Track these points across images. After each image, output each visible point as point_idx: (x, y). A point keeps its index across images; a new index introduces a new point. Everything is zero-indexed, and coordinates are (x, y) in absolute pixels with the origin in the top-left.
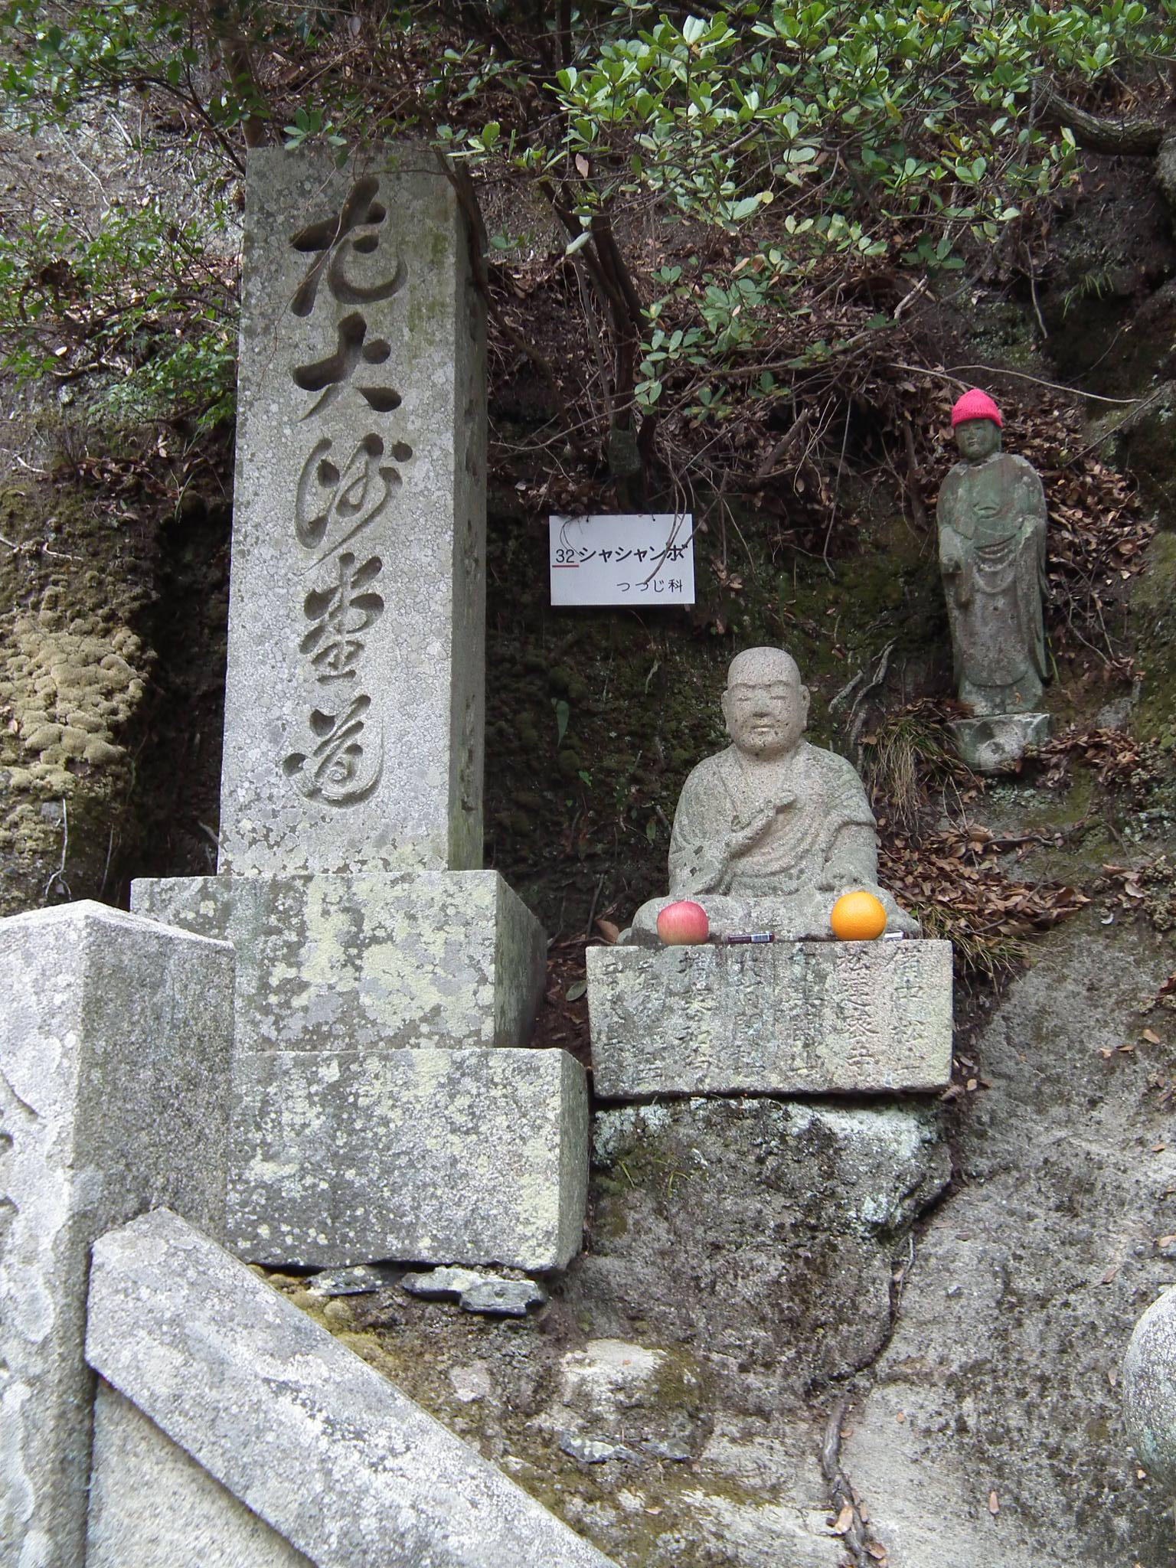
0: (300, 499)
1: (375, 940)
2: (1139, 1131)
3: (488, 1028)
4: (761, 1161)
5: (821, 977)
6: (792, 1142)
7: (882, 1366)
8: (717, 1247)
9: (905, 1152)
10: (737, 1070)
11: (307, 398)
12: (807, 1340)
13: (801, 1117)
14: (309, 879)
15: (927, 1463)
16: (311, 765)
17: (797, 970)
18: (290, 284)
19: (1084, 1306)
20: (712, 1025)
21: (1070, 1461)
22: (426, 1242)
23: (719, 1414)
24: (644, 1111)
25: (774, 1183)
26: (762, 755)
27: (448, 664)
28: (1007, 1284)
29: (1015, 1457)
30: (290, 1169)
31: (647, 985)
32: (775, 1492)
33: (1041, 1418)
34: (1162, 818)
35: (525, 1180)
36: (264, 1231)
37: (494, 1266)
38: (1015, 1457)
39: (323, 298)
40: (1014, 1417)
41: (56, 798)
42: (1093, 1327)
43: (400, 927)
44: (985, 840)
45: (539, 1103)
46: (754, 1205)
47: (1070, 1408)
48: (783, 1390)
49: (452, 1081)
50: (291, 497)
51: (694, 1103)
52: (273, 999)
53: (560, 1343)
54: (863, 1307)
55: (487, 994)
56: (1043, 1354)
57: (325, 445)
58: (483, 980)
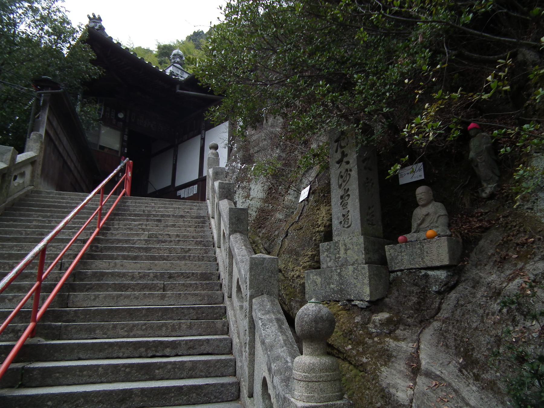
3: (364, 261)
4: (414, 281)
5: (423, 247)
7: (435, 318)
8: (406, 296)
10: (411, 264)
11: (338, 165)
13: (423, 272)
16: (343, 223)
18: (335, 149)
20: (406, 257)
25: (416, 285)
26: (424, 206)
29: (448, 335)
32: (404, 340)
37: (362, 300)
38: (448, 335)
39: (339, 149)
40: (450, 328)
41: (322, 232)
42: (469, 311)
43: (351, 246)
45: (95, 295)
51: (405, 271)
53: (373, 313)
55: (364, 256)
57: (341, 172)
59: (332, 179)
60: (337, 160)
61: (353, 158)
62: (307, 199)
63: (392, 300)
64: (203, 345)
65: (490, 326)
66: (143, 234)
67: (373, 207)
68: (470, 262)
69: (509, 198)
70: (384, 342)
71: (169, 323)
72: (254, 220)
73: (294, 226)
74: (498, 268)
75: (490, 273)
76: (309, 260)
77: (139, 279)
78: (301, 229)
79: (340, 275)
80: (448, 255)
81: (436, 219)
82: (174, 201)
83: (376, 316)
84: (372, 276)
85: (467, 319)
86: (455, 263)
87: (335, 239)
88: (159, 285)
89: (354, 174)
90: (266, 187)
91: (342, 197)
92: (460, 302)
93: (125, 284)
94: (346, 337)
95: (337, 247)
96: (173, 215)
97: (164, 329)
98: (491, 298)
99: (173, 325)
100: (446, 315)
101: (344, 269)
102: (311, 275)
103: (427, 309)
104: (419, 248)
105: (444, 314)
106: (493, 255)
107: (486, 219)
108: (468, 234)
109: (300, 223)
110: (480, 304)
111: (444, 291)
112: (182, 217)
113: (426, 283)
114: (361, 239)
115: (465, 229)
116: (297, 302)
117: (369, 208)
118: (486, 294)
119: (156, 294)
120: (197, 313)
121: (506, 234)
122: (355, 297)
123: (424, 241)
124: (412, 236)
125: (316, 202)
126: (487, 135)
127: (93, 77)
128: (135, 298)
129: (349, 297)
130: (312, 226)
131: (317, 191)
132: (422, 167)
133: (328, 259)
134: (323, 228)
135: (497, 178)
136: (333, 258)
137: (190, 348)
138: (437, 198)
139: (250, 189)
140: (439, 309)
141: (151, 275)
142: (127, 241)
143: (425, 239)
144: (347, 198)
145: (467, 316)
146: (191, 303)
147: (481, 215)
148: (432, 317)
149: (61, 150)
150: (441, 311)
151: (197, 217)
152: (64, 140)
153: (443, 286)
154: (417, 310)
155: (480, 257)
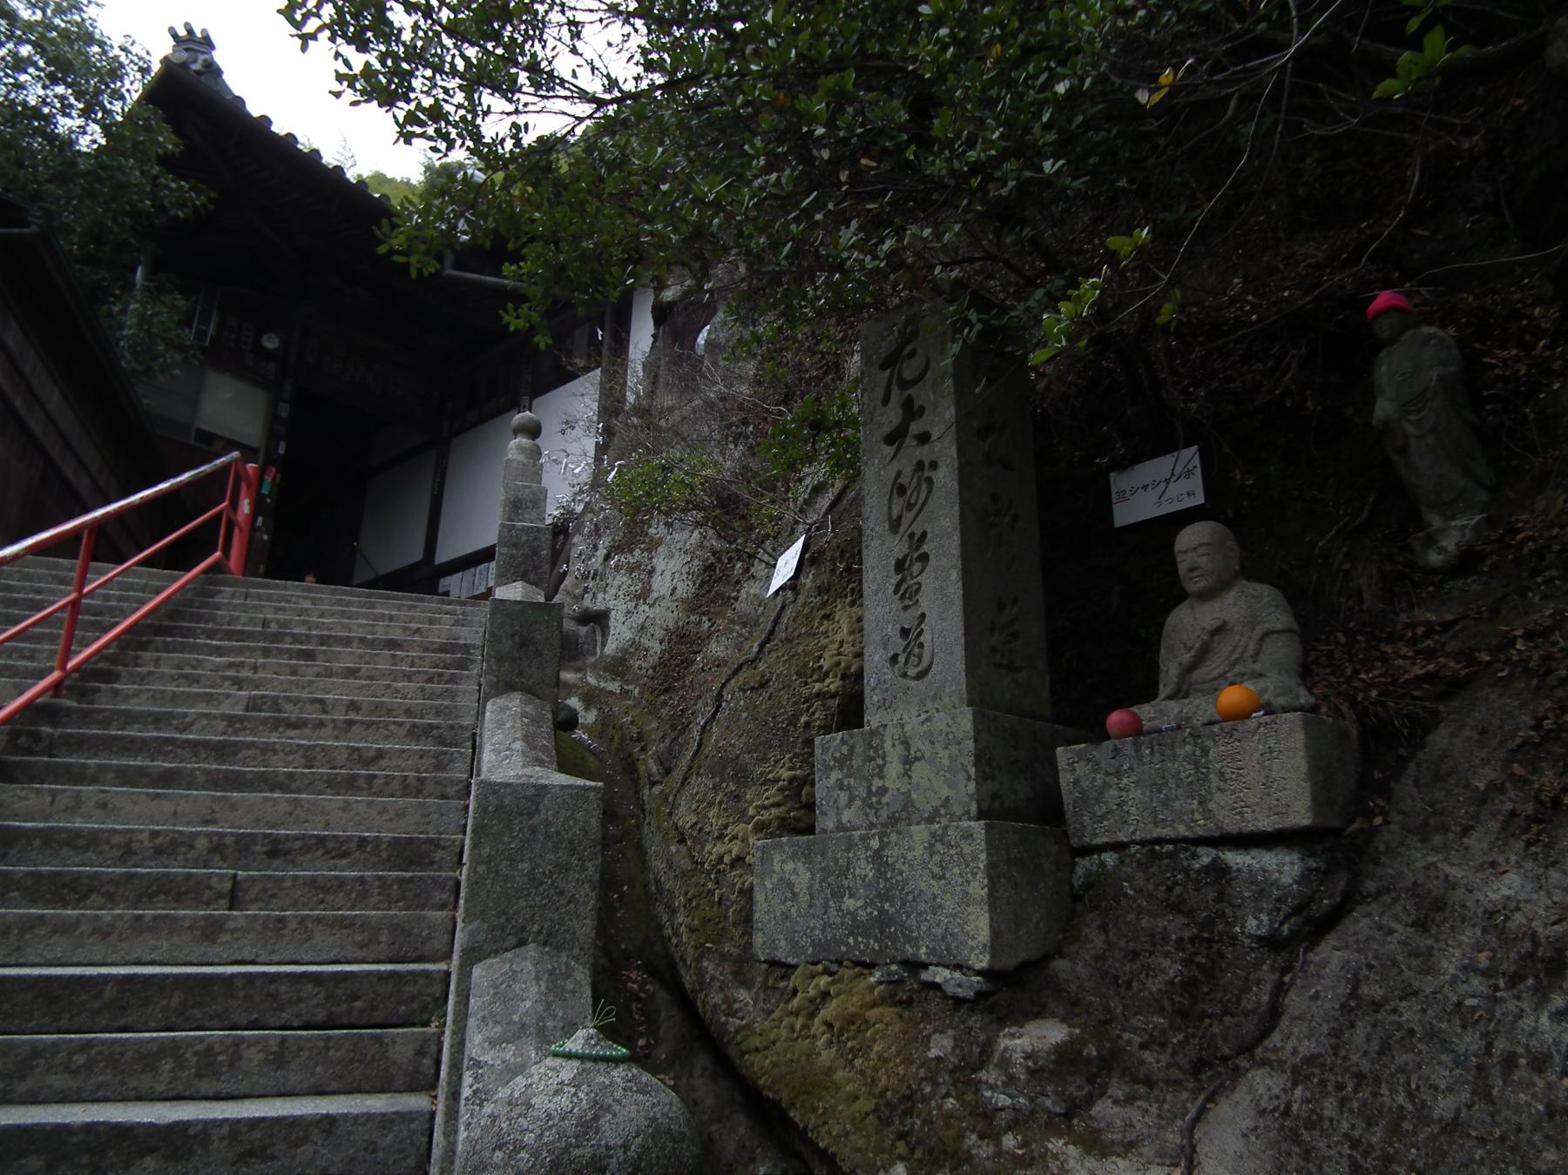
0: (890, 508)
1: (917, 759)
2: (1494, 855)
3: (974, 808)
4: (1170, 890)
5: (1205, 751)
6: (1193, 875)
7: (1259, 1051)
8: (1135, 955)
9: (1286, 880)
11: (889, 450)
12: (1196, 1027)
13: (1206, 856)
14: (885, 726)
15: (1253, 1139)
16: (902, 659)
17: (1188, 748)
18: (880, 391)
19: (1409, 1013)
20: (1136, 794)
21: (1366, 1154)
22: (923, 950)
23: (1115, 1081)
24: (1103, 856)
25: (1176, 907)
26: (1206, 596)
27: (960, 584)
28: (1354, 989)
30: (860, 903)
31: (1094, 771)
33: (1351, 1111)
34: (1554, 578)
35: (971, 909)
36: (851, 940)
37: (958, 967)
39: (895, 391)
40: (1329, 1108)
41: (833, 696)
42: (1412, 1032)
43: (926, 748)
44: (1427, 623)
45: (975, 858)
46: (1162, 923)
47: (1377, 1105)
48: (1168, 1066)
49: (931, 845)
50: (885, 509)
51: (1134, 848)
52: (874, 799)
53: (1002, 1021)
54: (1244, 1003)
55: (972, 786)
56: (1365, 1053)
57: (899, 474)
58: (969, 779)
59: (868, 500)
60: (887, 429)
61: (942, 417)
62: (793, 584)
63: (1081, 970)
64: (305, 1140)
65: (1525, 1120)
66: (228, 696)
67: (1014, 601)
68: (1396, 817)
69: (1549, 558)
70: (1043, 1156)
71: (190, 1043)
72: (654, 668)
73: (742, 676)
74: (1529, 844)
75: (1493, 865)
76: (778, 798)
77: (152, 858)
78: (764, 685)
79: (878, 858)
80: (1307, 785)
81: (1252, 647)
82: (380, 596)
83: (1012, 1036)
84: (1003, 867)
85: (1402, 1070)
86: (1335, 823)
87: (872, 719)
88: (214, 881)
89: (946, 477)
90: (696, 562)
91: (900, 566)
92: (1364, 990)
93: (77, 877)
94: (885, 1122)
95: (875, 752)
96: (362, 640)
97: (167, 1065)
98: (1514, 980)
99: (209, 1049)
100: (1308, 1047)
101: (894, 837)
102: (777, 857)
103: (1225, 1013)
104: (1189, 758)
105: (1296, 1038)
106: (1496, 788)
107: (1448, 649)
108: (1382, 703)
109: (762, 666)
110: (1459, 1005)
111: (1294, 936)
112: (393, 644)
113: (1219, 899)
114: (965, 721)
115: (1369, 685)
116: (724, 957)
117: (1001, 607)
118: (1483, 959)
119: (184, 917)
120: (329, 997)
121: (1548, 704)
122: (932, 951)
123: (1207, 730)
124: (1161, 712)
125: (820, 590)
126: (1441, 333)
127: (172, 212)
128: (95, 931)
129: (909, 950)
130: (799, 674)
131: (828, 555)
132: (1197, 461)
133: (843, 797)
134: (838, 683)
135: (1483, 496)
136: (861, 791)
137: (250, 1153)
138: (1253, 567)
139: (651, 572)
140: (1273, 1015)
141: (202, 843)
142: (158, 720)
143: (1211, 723)
144: (917, 567)
145: (1402, 1058)
146: (325, 957)
147: (1429, 633)
148: (1247, 1049)
149: (36, 425)
150: (1284, 1023)
151: (443, 648)
152: (54, 398)
153: (1287, 917)
154: (1184, 1016)
155: (1440, 795)
